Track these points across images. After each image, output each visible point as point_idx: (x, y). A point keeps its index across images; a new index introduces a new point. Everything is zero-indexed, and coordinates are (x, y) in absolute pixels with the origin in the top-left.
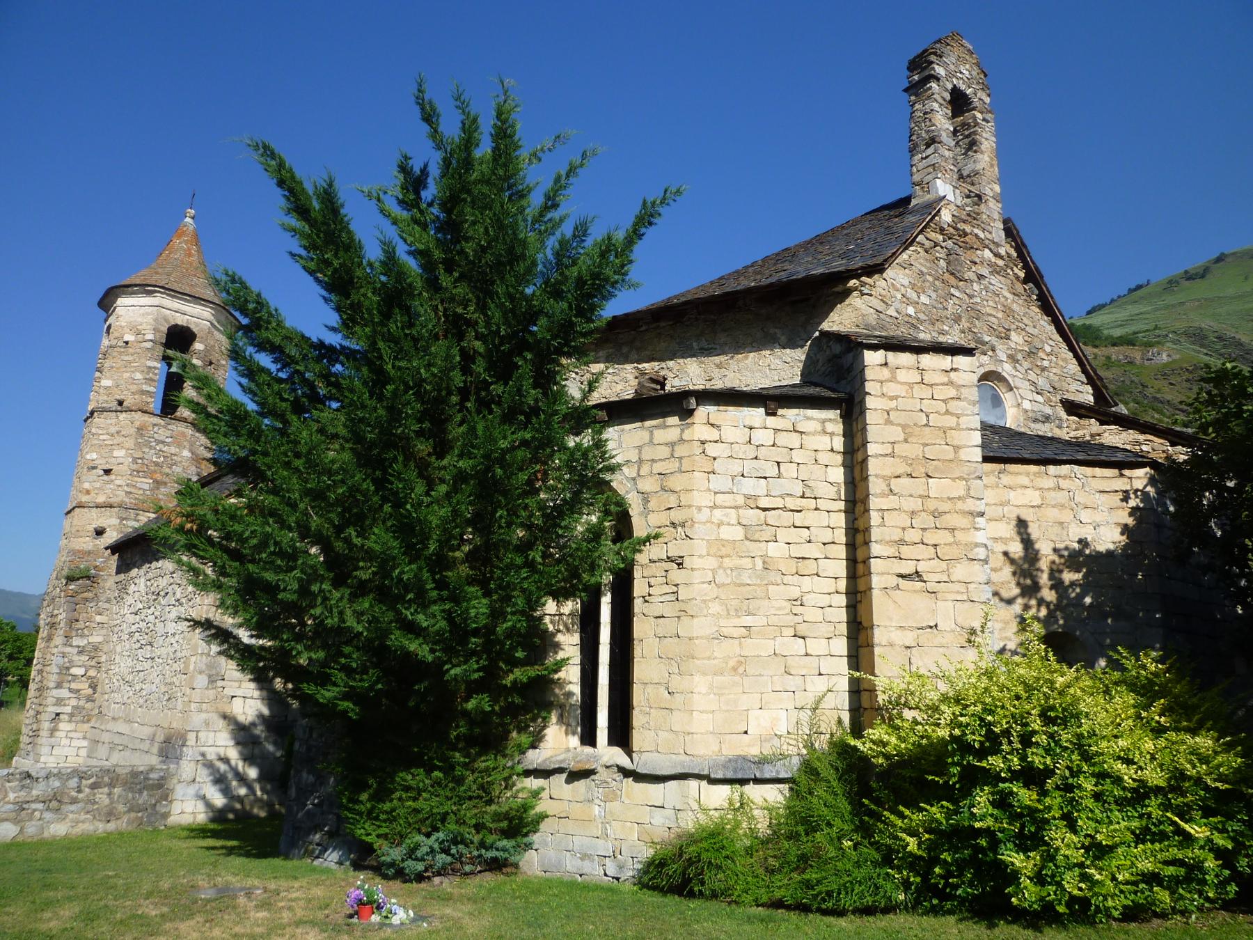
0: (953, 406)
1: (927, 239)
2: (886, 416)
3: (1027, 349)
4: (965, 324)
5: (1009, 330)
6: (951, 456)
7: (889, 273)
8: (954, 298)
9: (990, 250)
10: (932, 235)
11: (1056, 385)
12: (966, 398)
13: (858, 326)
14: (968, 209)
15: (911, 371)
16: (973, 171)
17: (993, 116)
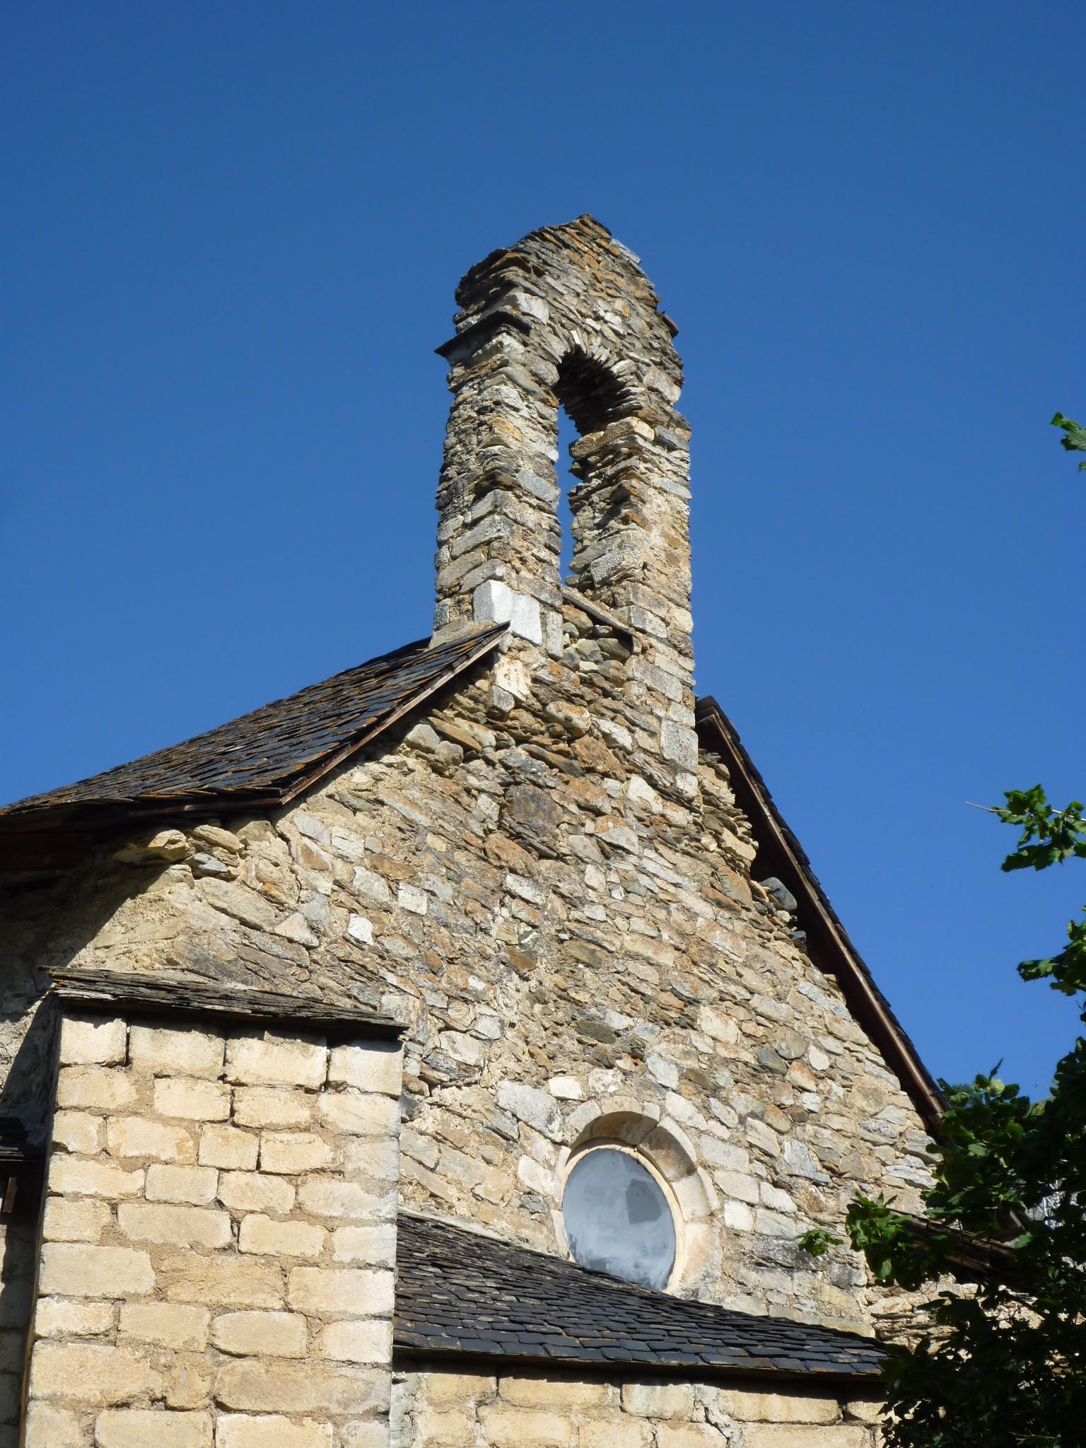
0: (318, 1194)
1: (443, 736)
2: (106, 1217)
3: (748, 1057)
4: (545, 975)
5: (694, 1002)
6: (297, 1345)
7: (298, 820)
8: (516, 906)
9: (650, 780)
10: (461, 728)
11: (843, 1164)
12: (359, 1171)
13: (171, 962)
14: (586, 666)
15: (201, 1086)
16: (616, 570)
17: (686, 435)
